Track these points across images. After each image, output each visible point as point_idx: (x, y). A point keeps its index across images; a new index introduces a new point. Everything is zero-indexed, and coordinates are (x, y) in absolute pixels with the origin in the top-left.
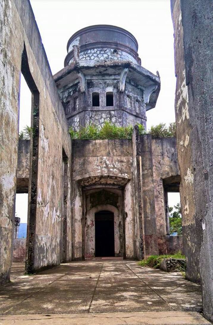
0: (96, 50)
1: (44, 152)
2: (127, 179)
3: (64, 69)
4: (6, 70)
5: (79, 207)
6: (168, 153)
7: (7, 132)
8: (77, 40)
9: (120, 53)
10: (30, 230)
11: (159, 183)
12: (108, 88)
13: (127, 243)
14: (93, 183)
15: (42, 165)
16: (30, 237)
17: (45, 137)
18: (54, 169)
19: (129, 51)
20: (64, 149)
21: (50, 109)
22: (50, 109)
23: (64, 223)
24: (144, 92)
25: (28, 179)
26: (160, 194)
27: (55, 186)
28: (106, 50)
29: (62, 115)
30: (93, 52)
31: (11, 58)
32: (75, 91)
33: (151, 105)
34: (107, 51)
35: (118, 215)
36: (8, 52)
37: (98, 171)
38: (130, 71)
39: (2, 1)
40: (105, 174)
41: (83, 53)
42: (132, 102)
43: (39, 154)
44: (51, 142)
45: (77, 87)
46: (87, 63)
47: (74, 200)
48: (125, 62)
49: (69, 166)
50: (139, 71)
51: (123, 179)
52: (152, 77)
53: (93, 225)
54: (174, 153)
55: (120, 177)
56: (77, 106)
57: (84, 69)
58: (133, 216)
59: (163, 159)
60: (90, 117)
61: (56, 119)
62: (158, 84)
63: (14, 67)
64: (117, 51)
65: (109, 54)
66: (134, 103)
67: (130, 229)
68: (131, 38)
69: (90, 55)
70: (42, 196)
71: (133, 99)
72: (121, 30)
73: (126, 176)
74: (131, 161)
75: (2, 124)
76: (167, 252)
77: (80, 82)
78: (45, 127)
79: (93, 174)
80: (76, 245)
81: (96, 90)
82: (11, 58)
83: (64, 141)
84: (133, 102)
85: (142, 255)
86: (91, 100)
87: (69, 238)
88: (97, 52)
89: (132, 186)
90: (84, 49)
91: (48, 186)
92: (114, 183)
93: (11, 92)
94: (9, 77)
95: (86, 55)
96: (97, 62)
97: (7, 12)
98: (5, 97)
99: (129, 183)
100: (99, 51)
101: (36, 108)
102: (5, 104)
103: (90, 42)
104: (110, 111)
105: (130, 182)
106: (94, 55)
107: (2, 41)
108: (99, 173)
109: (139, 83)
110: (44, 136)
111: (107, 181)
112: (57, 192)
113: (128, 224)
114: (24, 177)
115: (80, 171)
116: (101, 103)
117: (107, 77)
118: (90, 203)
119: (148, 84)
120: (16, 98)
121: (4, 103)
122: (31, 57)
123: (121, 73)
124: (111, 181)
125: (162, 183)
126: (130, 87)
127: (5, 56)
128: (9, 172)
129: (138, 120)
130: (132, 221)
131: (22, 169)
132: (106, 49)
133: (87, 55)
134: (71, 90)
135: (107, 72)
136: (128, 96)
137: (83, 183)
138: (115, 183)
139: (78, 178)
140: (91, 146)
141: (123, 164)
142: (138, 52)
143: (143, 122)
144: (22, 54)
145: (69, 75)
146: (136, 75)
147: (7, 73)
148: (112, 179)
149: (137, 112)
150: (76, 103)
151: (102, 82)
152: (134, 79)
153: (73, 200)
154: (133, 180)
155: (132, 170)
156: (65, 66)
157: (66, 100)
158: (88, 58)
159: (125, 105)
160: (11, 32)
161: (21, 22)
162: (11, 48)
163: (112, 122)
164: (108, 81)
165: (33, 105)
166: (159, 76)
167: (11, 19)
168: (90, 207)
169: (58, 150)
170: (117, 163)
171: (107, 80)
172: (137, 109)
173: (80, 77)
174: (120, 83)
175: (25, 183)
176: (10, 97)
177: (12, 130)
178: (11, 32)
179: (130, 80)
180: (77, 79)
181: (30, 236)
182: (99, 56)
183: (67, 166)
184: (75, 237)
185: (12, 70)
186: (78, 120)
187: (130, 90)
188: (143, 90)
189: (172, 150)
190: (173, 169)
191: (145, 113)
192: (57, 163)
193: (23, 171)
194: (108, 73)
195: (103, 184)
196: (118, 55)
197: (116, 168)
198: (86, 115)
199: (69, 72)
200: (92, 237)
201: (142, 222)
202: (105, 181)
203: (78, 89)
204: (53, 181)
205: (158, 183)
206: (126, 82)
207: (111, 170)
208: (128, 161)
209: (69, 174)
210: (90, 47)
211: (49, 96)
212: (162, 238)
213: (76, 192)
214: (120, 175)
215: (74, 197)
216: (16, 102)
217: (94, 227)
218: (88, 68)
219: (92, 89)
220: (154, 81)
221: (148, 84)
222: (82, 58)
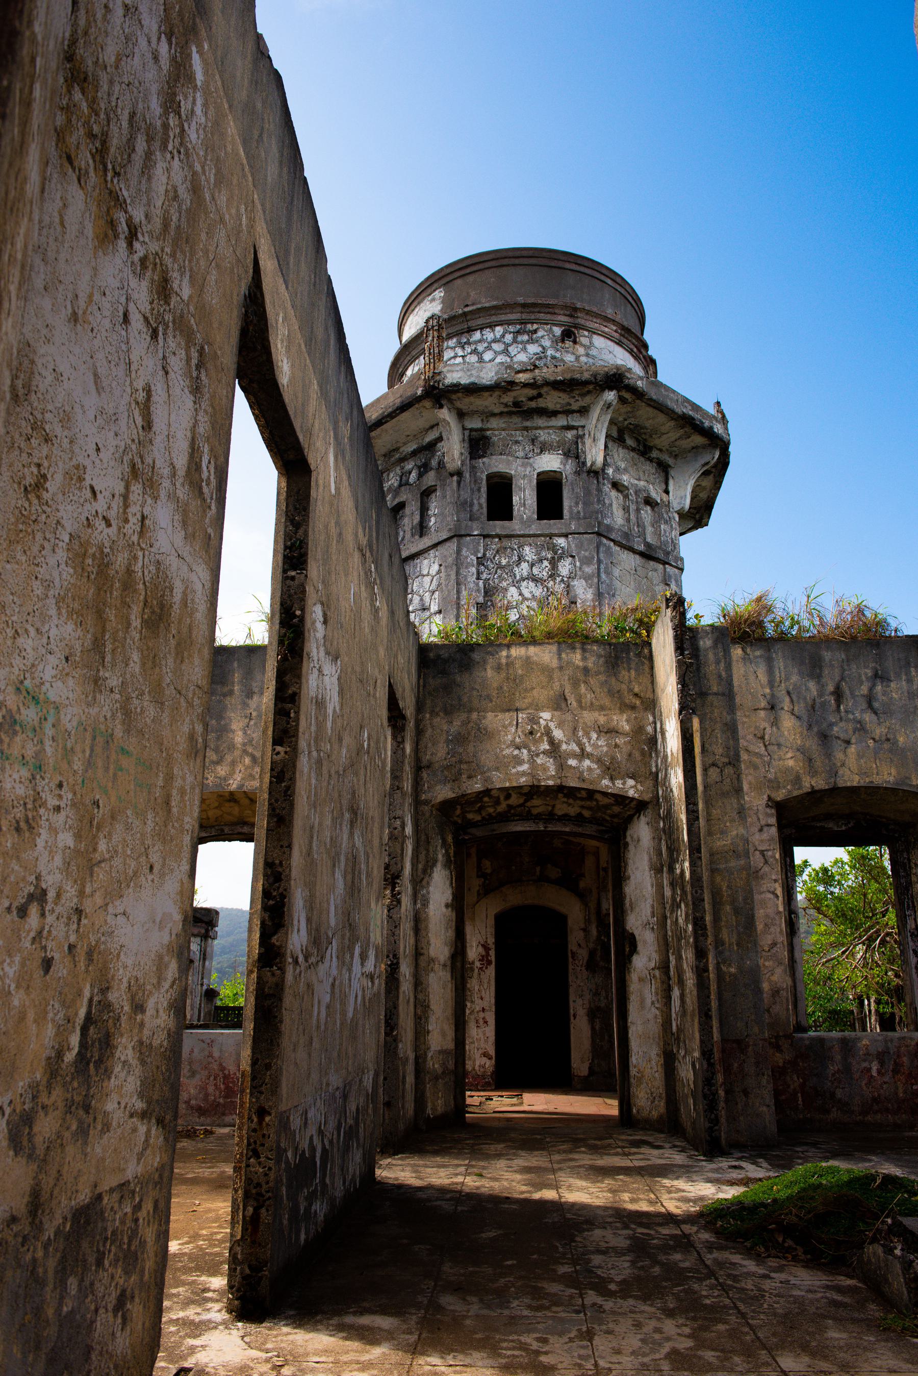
0: (499, 330)
1: (321, 718)
2: (633, 799)
3: (387, 394)
4: (164, 357)
5: (444, 909)
6: (792, 701)
7: (151, 661)
8: (433, 300)
9: (585, 341)
10: (251, 1094)
11: (761, 817)
12: (543, 456)
13: (634, 1060)
14: (499, 813)
15: (313, 781)
16: (255, 1130)
17: (328, 653)
18: (358, 780)
19: (616, 335)
20: (395, 687)
21: (349, 537)
22: (349, 537)
23: (386, 984)
24: (672, 472)
25: (251, 799)
26: (766, 862)
27: (361, 849)
28: (535, 331)
29: (391, 556)
30: (489, 335)
31: (192, 308)
32: (424, 469)
33: (694, 518)
34: (540, 333)
35: (583, 926)
36: (175, 275)
37: (521, 769)
38: (622, 400)
39: (159, 39)
40: (548, 779)
41: (455, 340)
42: (629, 507)
43: (300, 734)
44: (349, 670)
45: (433, 455)
46: (469, 373)
47: (424, 883)
48: (606, 369)
49: (408, 750)
50: (654, 401)
51: (616, 801)
52: (702, 423)
53: (489, 963)
54: (818, 701)
55: (605, 794)
56: (433, 520)
57: (460, 395)
58: (659, 951)
59: (775, 723)
60: (478, 558)
61: (368, 572)
62: (722, 445)
63: (202, 348)
64: (574, 334)
65: (547, 343)
66: (638, 510)
67: (648, 1002)
68: (623, 291)
69: (480, 348)
70: (309, 920)
71: (633, 497)
72: (586, 264)
73: (630, 788)
74: (649, 729)
75: (129, 624)
76: (800, 1102)
77: (445, 437)
78: (328, 613)
79: (499, 780)
80: (433, 1064)
81: (497, 464)
82: (192, 308)
83: (396, 656)
84: (633, 507)
85: (710, 1128)
86: (483, 501)
87: (406, 1048)
88: (503, 336)
89: (656, 829)
90: (458, 328)
91: (334, 866)
92: (580, 815)
93: (181, 462)
94: (176, 391)
95: (466, 346)
96: (506, 368)
97: (180, 97)
98: (151, 487)
99: (642, 817)
100: (512, 335)
101: (296, 533)
102: (147, 522)
103: (479, 306)
104: (551, 536)
105: (649, 811)
106: (495, 346)
107: (147, 216)
108: (524, 774)
109: (656, 441)
110: (322, 649)
111: (554, 806)
112: (367, 873)
113: (641, 980)
114: (234, 786)
115: (448, 767)
116: (519, 510)
117: (541, 422)
118: (478, 876)
119: (686, 444)
120: (205, 490)
121: (143, 518)
122: (281, 320)
123: (589, 406)
124: (569, 805)
125: (773, 820)
126: (621, 455)
127: (158, 293)
128: (151, 868)
129: (656, 570)
130: (657, 973)
131: (229, 758)
132: (535, 326)
133: (468, 349)
134: (409, 465)
135: (541, 403)
136: (616, 485)
137: (458, 812)
138: (587, 814)
139: (443, 793)
140: (492, 668)
141: (620, 741)
142: (647, 336)
143: (670, 577)
144: (242, 298)
145: (405, 415)
146: (645, 416)
147: (167, 373)
148: (576, 798)
149: (649, 540)
150: (428, 509)
151: (521, 438)
152: (636, 426)
153: (420, 881)
154: (658, 804)
155: (654, 765)
156: (391, 385)
157: (394, 498)
158: (474, 359)
159: (606, 516)
160: (195, 189)
161: (245, 162)
162: (190, 261)
163: (559, 576)
164: (543, 436)
165: (283, 520)
166: (724, 416)
167: (201, 132)
168: (479, 894)
169: (375, 694)
170: (594, 736)
171: (539, 431)
172: (649, 530)
173: (444, 420)
174: (588, 441)
175: (236, 810)
176: (178, 485)
177: (178, 644)
178: (195, 189)
179: (621, 432)
180: (432, 427)
181: (253, 1126)
182: (510, 349)
183: (403, 749)
184: (428, 1032)
185: (194, 362)
186: (435, 568)
187: (623, 466)
188: (669, 466)
189: (807, 689)
190: (818, 763)
191: (675, 545)
192: (368, 753)
193: (233, 763)
194: (543, 405)
195: (537, 818)
196: (577, 346)
197: (589, 756)
198: (464, 552)
199: (404, 407)
200: (483, 1010)
201: (709, 989)
202: (546, 805)
203: (434, 463)
204: (351, 834)
205: (759, 819)
206: (607, 437)
207: (572, 762)
208: (639, 730)
209: (407, 785)
210: (480, 321)
211: (346, 483)
212: (780, 1043)
213: (431, 849)
214: (606, 782)
215: (425, 871)
216: (204, 511)
217: (491, 971)
218: (473, 389)
219: (485, 460)
220: (708, 433)
221: (686, 444)
222: (450, 359)
